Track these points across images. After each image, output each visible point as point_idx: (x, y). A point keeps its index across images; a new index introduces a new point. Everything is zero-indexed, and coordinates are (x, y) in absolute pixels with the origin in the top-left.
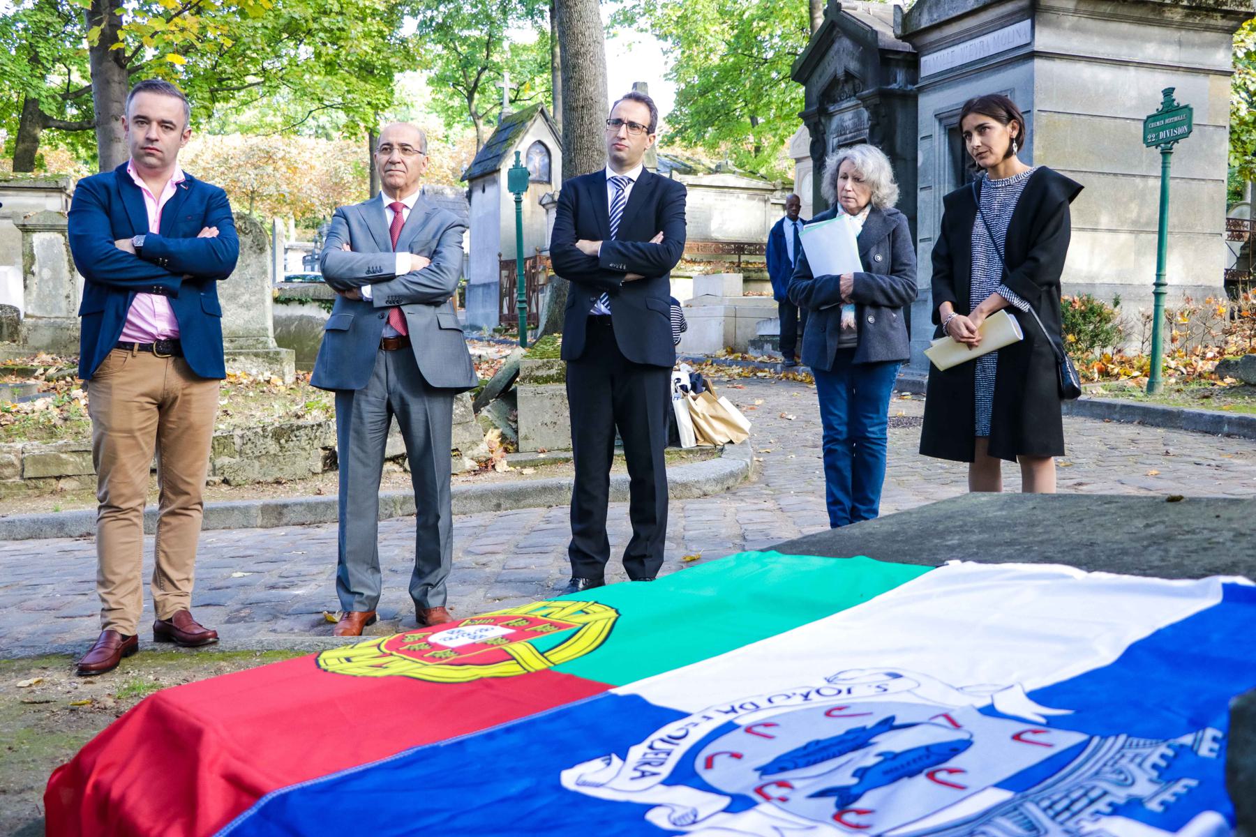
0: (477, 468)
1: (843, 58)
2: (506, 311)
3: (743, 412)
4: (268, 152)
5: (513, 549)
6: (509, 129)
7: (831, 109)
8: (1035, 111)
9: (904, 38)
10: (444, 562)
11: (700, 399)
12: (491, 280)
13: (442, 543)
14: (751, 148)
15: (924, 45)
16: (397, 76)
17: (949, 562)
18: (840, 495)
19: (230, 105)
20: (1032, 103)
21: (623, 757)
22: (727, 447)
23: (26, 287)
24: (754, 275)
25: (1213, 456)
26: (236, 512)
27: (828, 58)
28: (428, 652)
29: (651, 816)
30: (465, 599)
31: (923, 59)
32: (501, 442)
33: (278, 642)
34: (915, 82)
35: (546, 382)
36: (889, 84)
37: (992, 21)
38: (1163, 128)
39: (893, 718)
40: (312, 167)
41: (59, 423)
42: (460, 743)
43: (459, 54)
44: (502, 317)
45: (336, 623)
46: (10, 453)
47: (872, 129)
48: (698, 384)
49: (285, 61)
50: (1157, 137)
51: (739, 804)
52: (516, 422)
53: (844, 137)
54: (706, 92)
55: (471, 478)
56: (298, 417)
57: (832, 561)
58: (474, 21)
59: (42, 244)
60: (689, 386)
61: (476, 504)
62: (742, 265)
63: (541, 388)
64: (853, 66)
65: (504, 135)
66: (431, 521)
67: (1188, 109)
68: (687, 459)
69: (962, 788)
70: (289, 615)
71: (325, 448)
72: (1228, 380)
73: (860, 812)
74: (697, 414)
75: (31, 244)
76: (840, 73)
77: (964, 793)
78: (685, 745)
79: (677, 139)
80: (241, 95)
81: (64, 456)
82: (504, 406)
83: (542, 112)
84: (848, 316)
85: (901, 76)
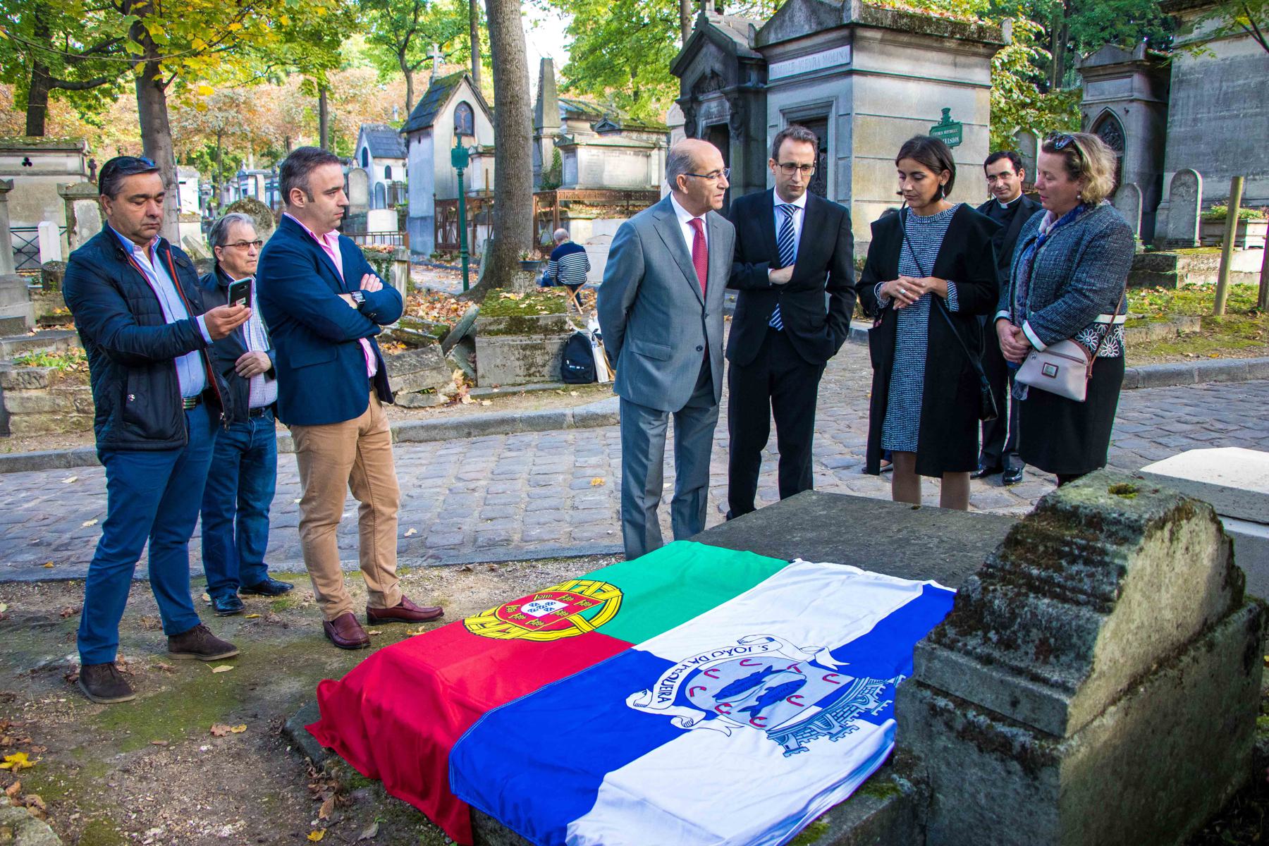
1: (709, 60)
2: (440, 240)
4: (232, 98)
5: (490, 476)
7: (701, 98)
9: (757, 49)
12: (426, 214)
14: (630, 92)
15: (772, 57)
20: (851, 108)
21: (652, 690)
27: (699, 58)
28: (526, 621)
29: (673, 722)
30: (467, 519)
31: (771, 66)
34: (766, 83)
35: (497, 334)
36: (745, 82)
39: (771, 667)
40: (269, 110)
42: (568, 681)
43: (392, 18)
44: (437, 245)
47: (732, 116)
51: (710, 716)
52: (474, 362)
54: (595, 50)
55: (444, 409)
57: (733, 552)
59: (81, 208)
61: (453, 433)
63: (494, 339)
64: (718, 67)
67: (959, 126)
69: (802, 705)
73: (761, 718)
75: (73, 209)
76: (708, 71)
77: (802, 708)
78: (679, 682)
83: (466, 78)
85: (754, 76)
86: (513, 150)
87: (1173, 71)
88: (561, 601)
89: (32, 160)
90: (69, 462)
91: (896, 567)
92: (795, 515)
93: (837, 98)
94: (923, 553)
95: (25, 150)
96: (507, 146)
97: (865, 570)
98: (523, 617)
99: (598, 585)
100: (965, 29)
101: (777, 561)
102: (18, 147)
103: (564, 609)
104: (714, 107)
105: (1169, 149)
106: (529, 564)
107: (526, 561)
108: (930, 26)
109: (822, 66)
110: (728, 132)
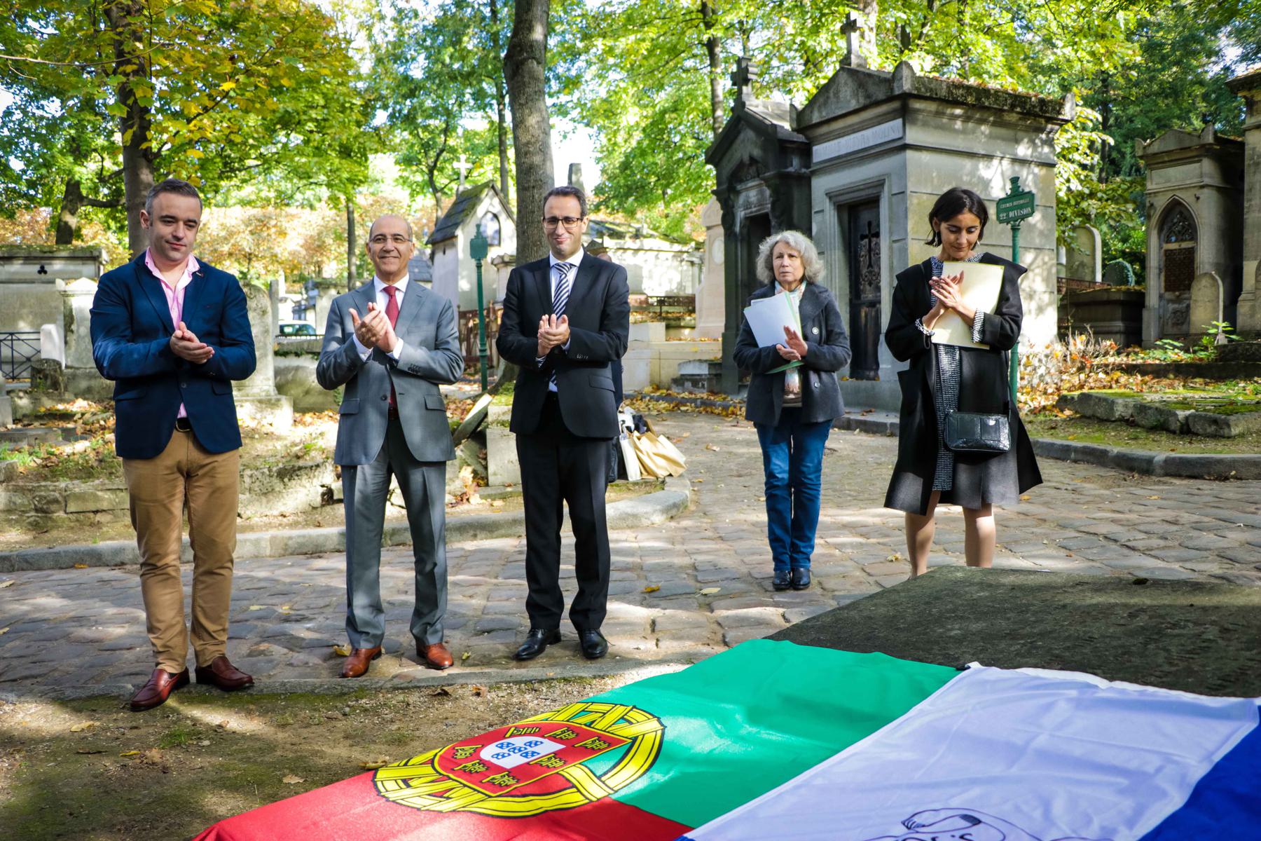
0: (454, 501)
1: (747, 146)
3: (674, 444)
6: (466, 203)
7: (739, 187)
8: (908, 192)
10: (441, 604)
11: (644, 438)
13: (438, 587)
15: (816, 137)
16: (371, 157)
17: (970, 664)
18: (779, 532)
19: (232, 183)
22: (668, 479)
23: (66, 343)
24: (673, 323)
25: (1066, 481)
26: (248, 544)
31: (815, 148)
32: (474, 478)
33: (299, 684)
34: (808, 166)
36: (787, 167)
37: (871, 119)
38: (1011, 209)
41: (95, 464)
43: (422, 139)
45: (345, 656)
46: (54, 491)
47: (773, 204)
48: (640, 424)
49: (279, 146)
50: (1008, 216)
52: (485, 459)
53: (749, 211)
56: (298, 457)
58: (435, 113)
60: (633, 427)
62: (664, 315)
65: (462, 207)
66: (428, 568)
68: (633, 491)
70: (303, 648)
71: (323, 486)
72: (1068, 412)
74: (641, 452)
76: (746, 159)
79: (602, 207)
80: (242, 175)
81: (100, 493)
82: (474, 446)
83: (493, 187)
84: (794, 381)
85: (796, 162)
86: (536, 237)
87: (1248, 153)
88: (554, 739)
89: (47, 268)
90: (13, 566)
91: (1167, 674)
92: (937, 598)
93: (889, 175)
94: (1205, 649)
95: (42, 258)
96: (530, 232)
97: (1111, 679)
98: (481, 769)
99: (620, 711)
100: (1025, 103)
101: (934, 668)
102: (34, 254)
103: (556, 754)
104: (753, 195)
105: (1247, 236)
106: (530, 686)
107: (526, 682)
108: (988, 98)
109: (871, 144)
110: (769, 222)
